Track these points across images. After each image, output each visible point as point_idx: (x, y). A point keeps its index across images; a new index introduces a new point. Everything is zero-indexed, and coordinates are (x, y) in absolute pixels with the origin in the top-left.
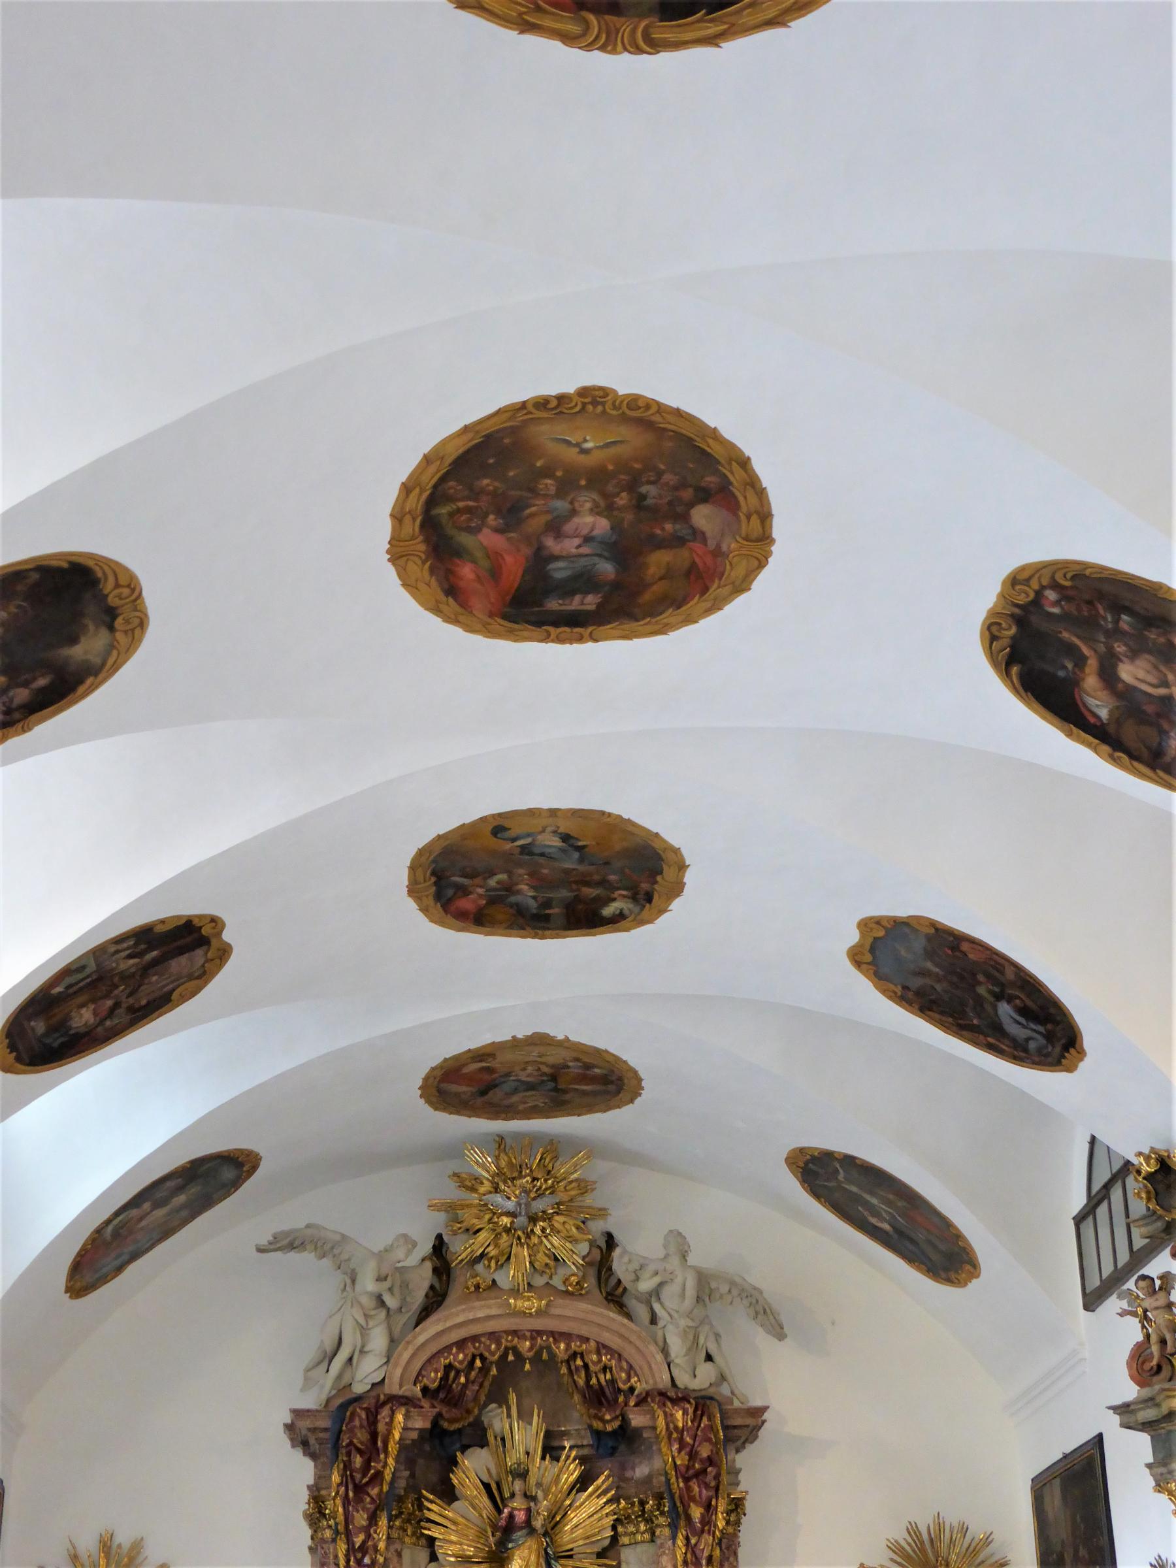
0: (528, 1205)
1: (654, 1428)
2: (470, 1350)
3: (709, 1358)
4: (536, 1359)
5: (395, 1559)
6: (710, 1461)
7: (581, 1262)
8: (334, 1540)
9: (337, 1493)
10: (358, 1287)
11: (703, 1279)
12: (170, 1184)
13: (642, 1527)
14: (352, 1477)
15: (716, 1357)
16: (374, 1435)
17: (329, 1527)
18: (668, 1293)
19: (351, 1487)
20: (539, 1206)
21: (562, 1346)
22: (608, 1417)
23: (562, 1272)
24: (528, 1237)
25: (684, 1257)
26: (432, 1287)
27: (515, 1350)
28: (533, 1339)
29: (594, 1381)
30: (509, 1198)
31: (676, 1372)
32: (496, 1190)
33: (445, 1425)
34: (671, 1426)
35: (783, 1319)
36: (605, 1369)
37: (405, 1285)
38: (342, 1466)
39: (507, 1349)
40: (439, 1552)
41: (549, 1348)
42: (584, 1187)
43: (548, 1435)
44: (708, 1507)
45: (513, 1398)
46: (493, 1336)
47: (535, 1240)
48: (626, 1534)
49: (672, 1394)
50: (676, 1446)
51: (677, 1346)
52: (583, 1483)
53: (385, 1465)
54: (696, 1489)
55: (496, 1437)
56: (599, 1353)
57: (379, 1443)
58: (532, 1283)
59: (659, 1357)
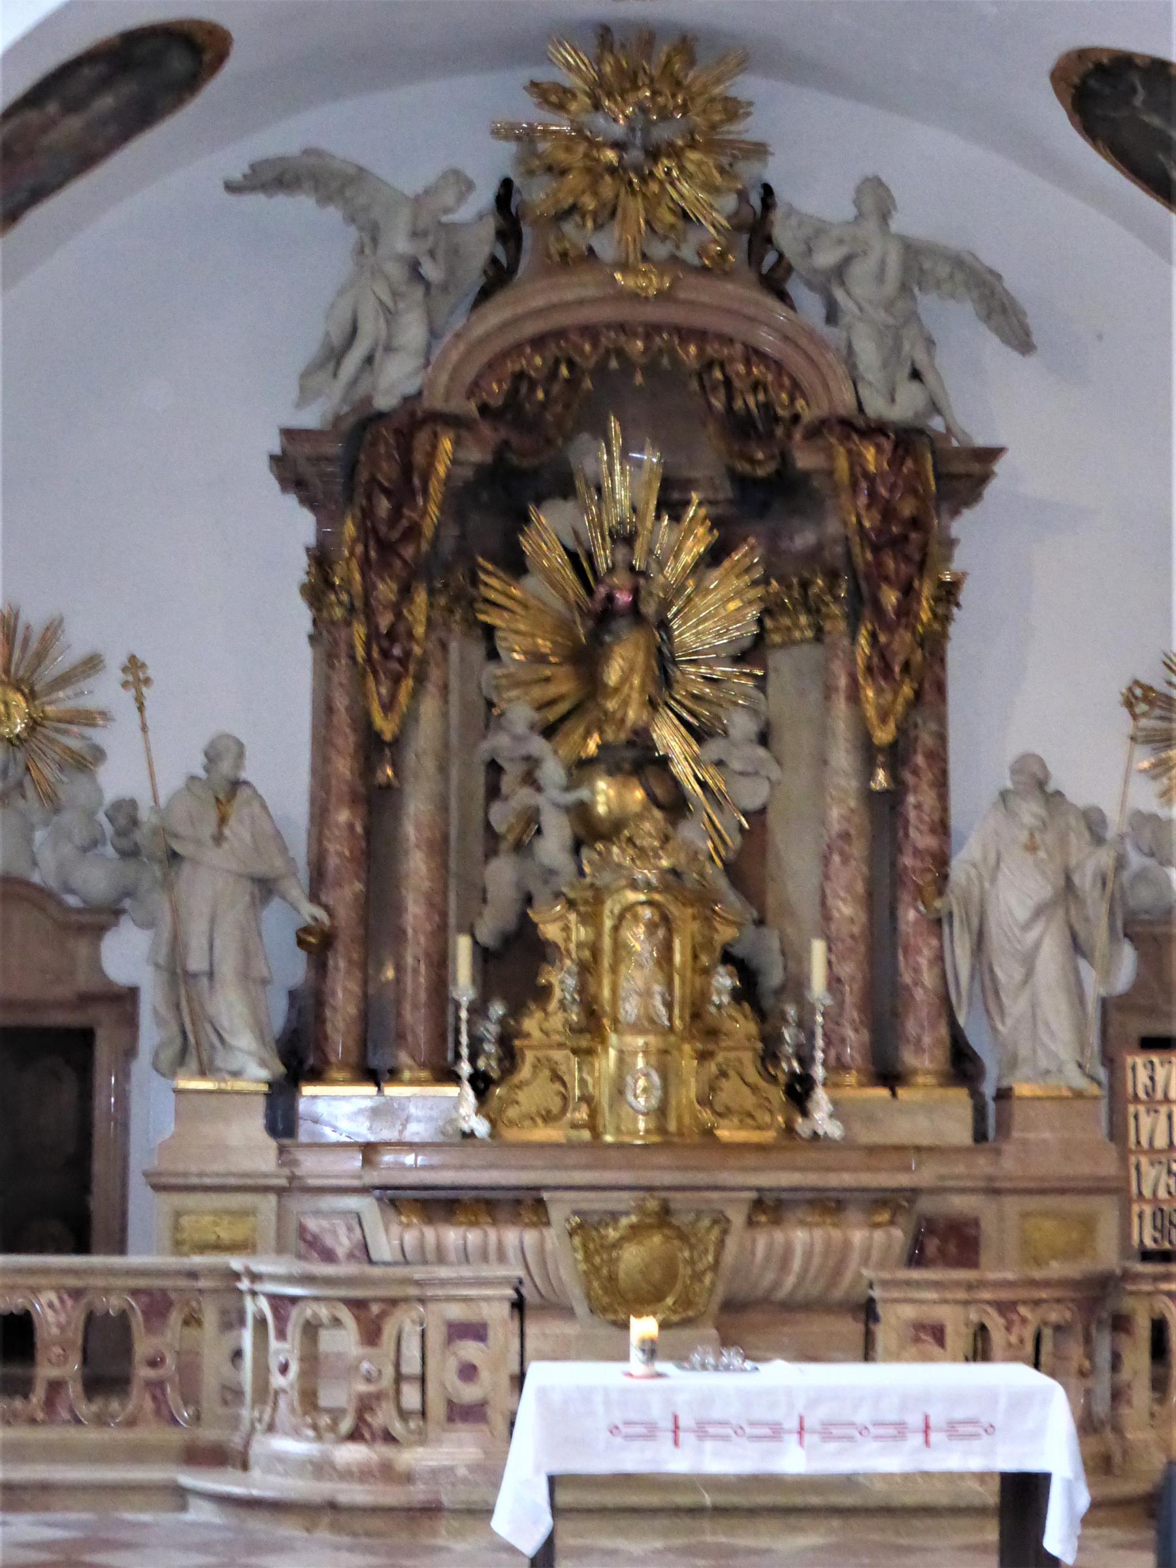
0: (646, 131)
1: (830, 473)
2: (552, 350)
3: (916, 375)
4: (651, 369)
5: (438, 655)
6: (916, 523)
7: (725, 223)
8: (348, 624)
9: (352, 553)
10: (382, 251)
11: (912, 251)
12: (88, 73)
13: (803, 620)
14: (375, 531)
15: (929, 377)
16: (407, 469)
17: (340, 603)
18: (861, 271)
19: (372, 543)
20: (662, 133)
21: (693, 349)
22: (760, 456)
23: (693, 239)
24: (644, 180)
25: (885, 217)
26: (494, 260)
27: (620, 353)
28: (648, 337)
29: (738, 404)
30: (616, 120)
31: (864, 392)
32: (597, 106)
33: (514, 459)
34: (858, 469)
35: (1032, 322)
36: (756, 386)
37: (454, 252)
38: (358, 514)
39: (608, 352)
40: (501, 645)
41: (672, 353)
42: (734, 109)
43: (667, 484)
44: (908, 591)
45: (614, 425)
46: (590, 332)
47: (654, 187)
48: (777, 630)
49: (860, 422)
50: (863, 500)
51: (868, 354)
52: (714, 556)
53: (425, 512)
54: (891, 565)
55: (588, 487)
56: (748, 363)
57: (416, 481)
58: (649, 254)
59: (841, 370)
